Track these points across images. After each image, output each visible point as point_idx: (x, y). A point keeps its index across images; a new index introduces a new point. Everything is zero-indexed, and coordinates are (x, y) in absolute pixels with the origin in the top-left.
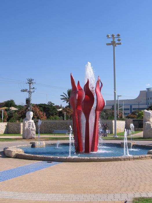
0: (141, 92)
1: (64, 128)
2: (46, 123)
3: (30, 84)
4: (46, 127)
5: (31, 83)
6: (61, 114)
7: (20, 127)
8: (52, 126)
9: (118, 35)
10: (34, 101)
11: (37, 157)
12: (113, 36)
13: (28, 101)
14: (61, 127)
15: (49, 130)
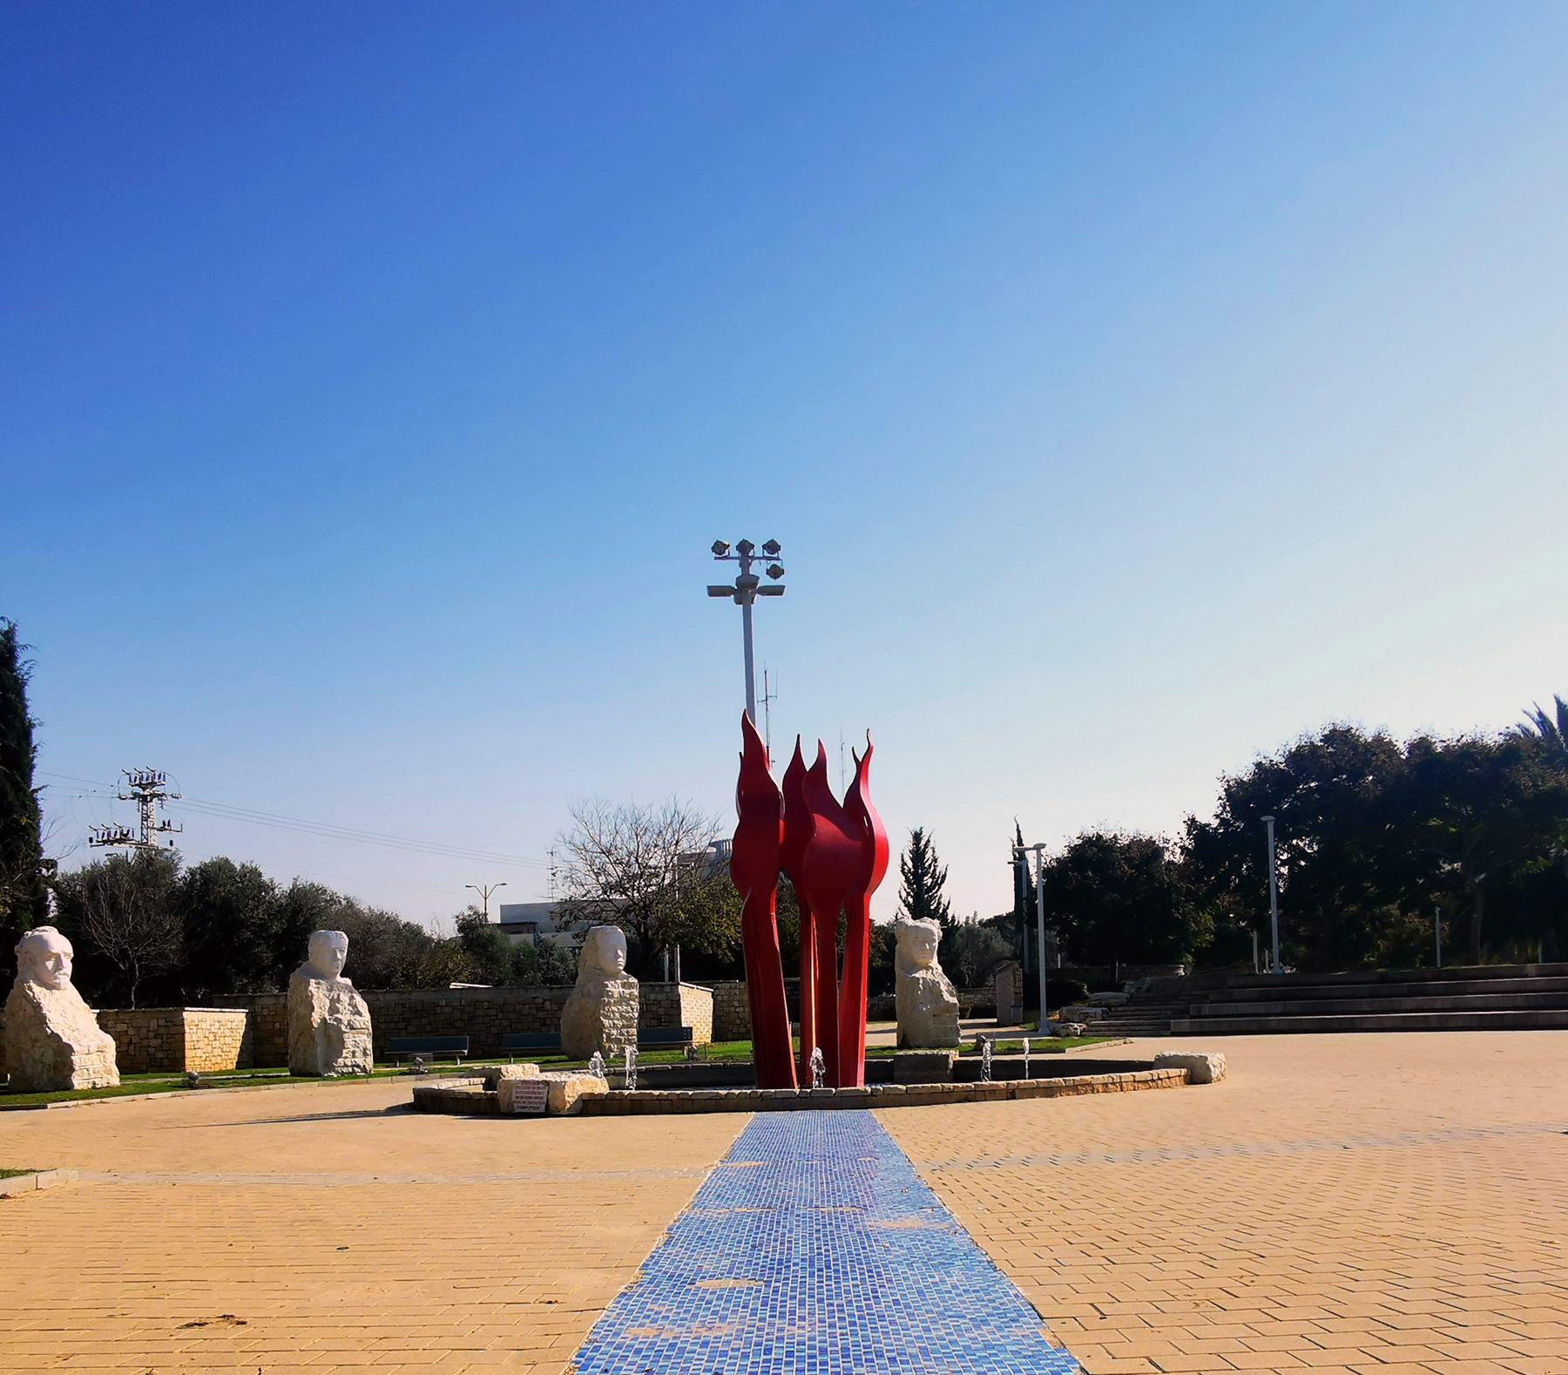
0: (1259, 765)
5: (153, 796)
7: (183, 1034)
9: (772, 547)
11: (721, 1098)
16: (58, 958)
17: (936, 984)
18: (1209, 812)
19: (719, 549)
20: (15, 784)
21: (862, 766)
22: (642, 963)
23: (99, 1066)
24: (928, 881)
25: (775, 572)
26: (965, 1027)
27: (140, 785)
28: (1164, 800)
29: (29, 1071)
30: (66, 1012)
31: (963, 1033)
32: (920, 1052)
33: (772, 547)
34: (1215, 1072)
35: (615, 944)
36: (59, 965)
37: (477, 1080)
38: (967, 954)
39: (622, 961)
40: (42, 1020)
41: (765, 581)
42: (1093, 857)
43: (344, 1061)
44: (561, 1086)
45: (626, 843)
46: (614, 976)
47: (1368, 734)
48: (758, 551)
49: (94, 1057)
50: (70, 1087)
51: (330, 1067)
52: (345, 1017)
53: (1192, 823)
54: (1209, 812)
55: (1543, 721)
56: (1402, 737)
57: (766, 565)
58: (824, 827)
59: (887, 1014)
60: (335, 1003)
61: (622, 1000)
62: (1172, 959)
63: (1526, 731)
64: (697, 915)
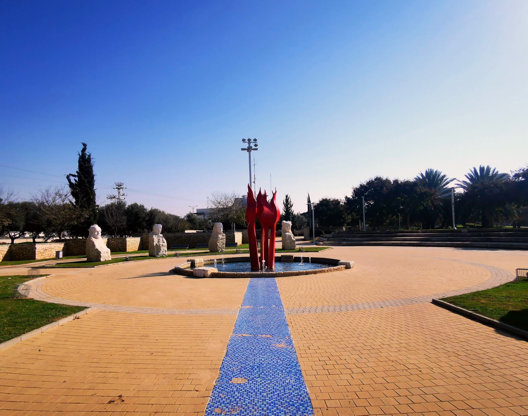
0: (361, 185)
3: (119, 189)
12: (249, 140)
16: (98, 232)
17: (290, 236)
18: (350, 195)
19: (244, 140)
20: (90, 188)
21: (274, 195)
22: (227, 228)
23: (107, 256)
24: (289, 206)
25: (256, 145)
26: (297, 240)
28: (342, 192)
30: (100, 243)
31: (297, 243)
33: (255, 140)
34: (352, 266)
35: (220, 226)
36: (98, 233)
38: (298, 222)
39: (222, 230)
40: (94, 246)
41: (254, 147)
42: (325, 203)
43: (161, 253)
44: (207, 271)
45: (223, 201)
46: (220, 234)
47: (384, 178)
48: (252, 141)
49: (106, 254)
50: (100, 261)
51: (158, 254)
52: (161, 243)
53: (346, 197)
54: (350, 195)
55: (422, 175)
56: (392, 179)
57: (254, 144)
58: (266, 209)
59: (280, 235)
60: (159, 240)
61: (222, 239)
62: (342, 225)
63: (418, 177)
64: (239, 217)
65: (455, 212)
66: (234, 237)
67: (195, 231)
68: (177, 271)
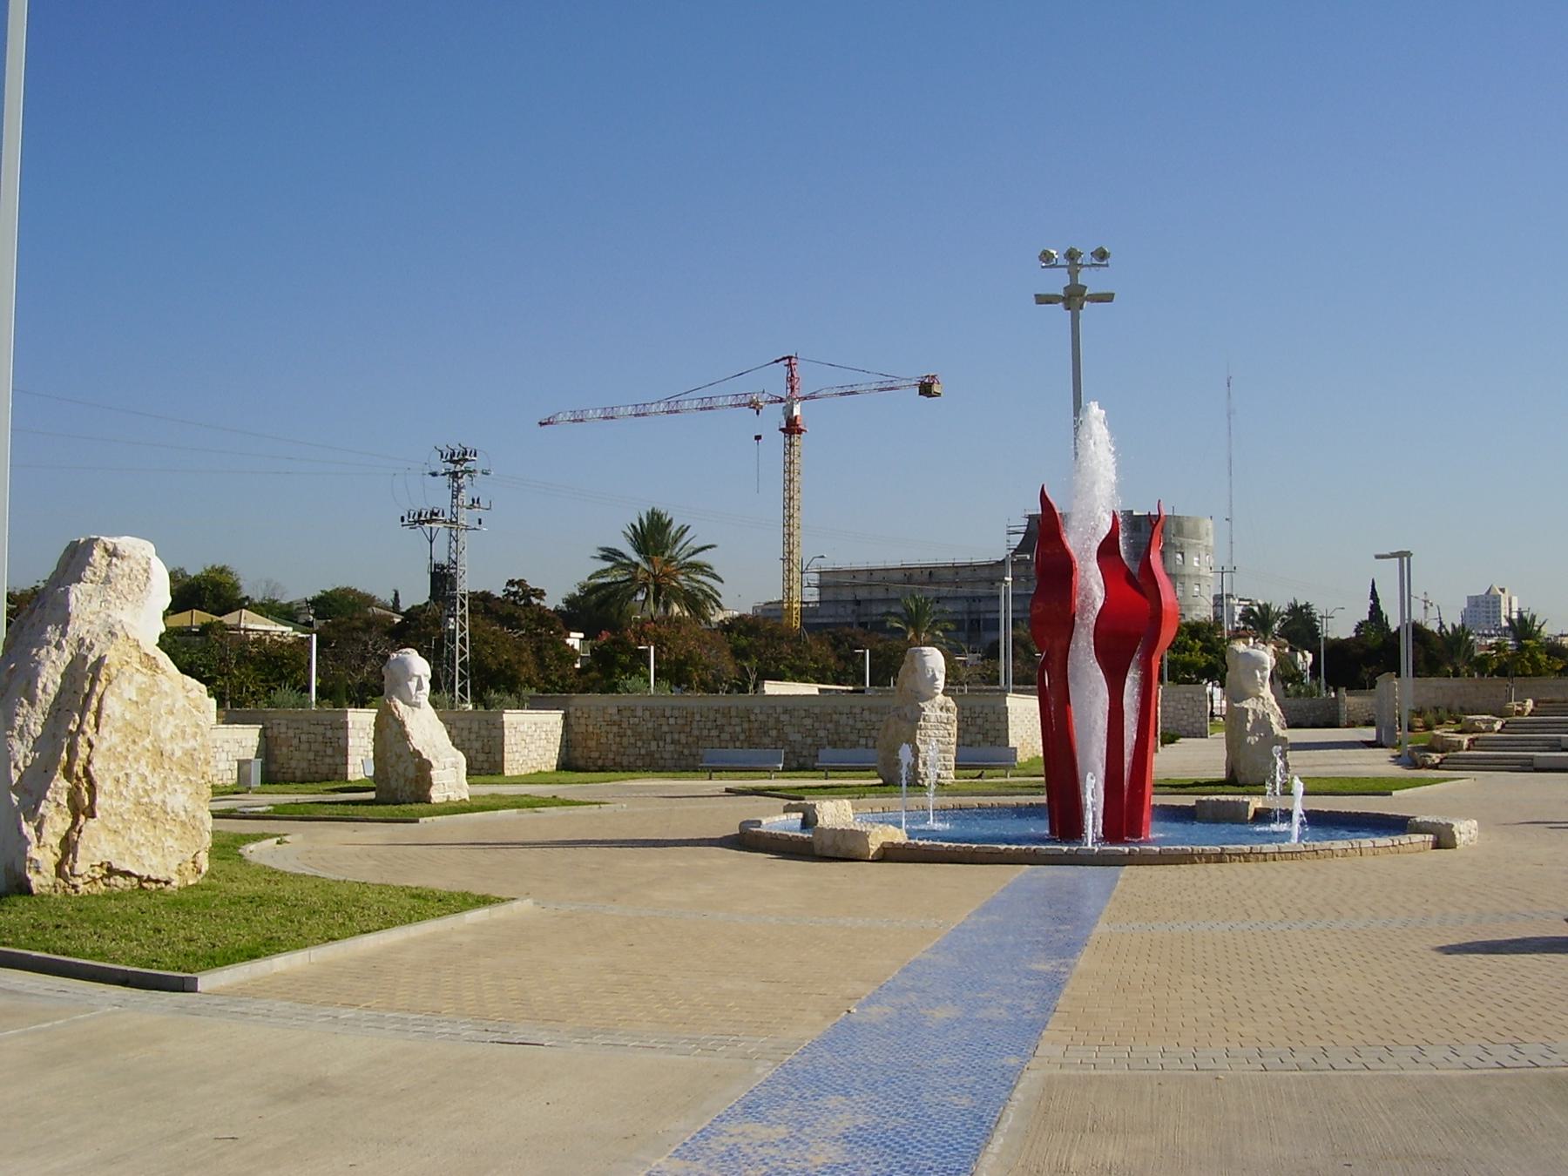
1: (734, 738)
2: (627, 713)
4: (629, 732)
6: (1481, 665)
7: (347, 738)
8: (665, 728)
9: (1102, 255)
10: (468, 583)
12: (1072, 255)
13: (442, 579)
14: (714, 733)
15: (643, 751)
27: (451, 461)
29: (393, 784)
32: (1223, 798)
36: (420, 687)
37: (794, 815)
48: (1086, 258)
49: (449, 770)
65: (318, 675)
66: (1001, 717)
67: (812, 689)
68: (747, 840)
